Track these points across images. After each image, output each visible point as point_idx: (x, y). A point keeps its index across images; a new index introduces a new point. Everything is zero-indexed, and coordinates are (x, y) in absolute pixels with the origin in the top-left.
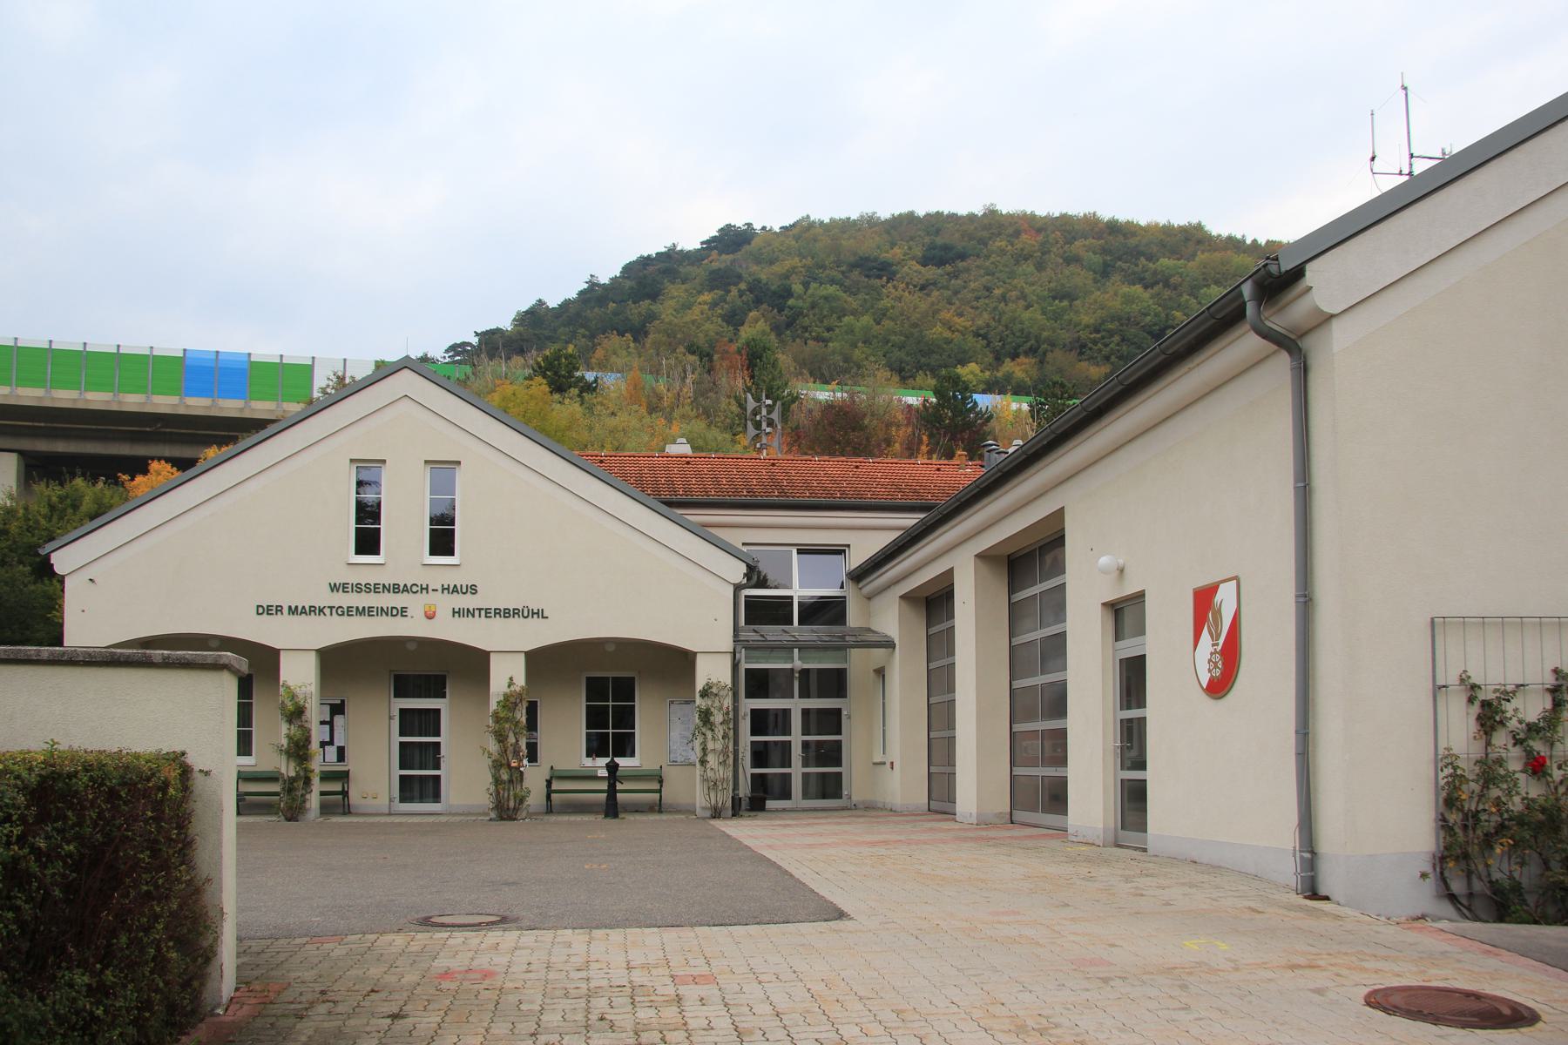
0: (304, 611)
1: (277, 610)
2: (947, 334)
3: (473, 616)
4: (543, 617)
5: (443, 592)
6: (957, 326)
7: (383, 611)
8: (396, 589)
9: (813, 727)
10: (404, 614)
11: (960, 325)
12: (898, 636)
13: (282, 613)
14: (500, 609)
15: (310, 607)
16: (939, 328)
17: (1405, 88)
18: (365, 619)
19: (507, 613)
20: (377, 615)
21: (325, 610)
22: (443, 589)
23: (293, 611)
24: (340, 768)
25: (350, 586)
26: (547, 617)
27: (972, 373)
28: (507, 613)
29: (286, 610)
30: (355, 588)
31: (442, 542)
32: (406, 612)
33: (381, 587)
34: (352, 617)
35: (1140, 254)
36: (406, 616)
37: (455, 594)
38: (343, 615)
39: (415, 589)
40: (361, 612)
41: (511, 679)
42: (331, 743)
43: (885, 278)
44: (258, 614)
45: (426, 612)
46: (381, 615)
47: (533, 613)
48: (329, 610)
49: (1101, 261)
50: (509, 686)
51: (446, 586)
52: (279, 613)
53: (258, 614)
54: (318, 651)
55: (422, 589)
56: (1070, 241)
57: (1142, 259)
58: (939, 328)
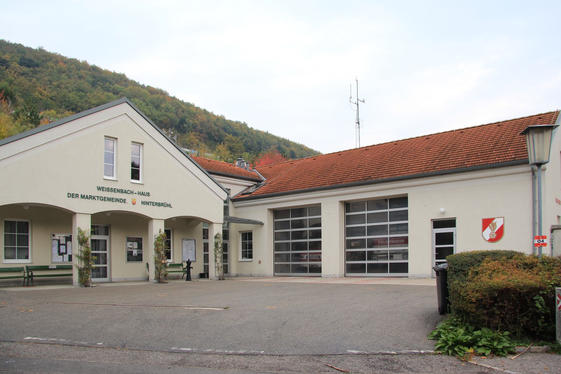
0: (87, 198)
1: (76, 196)
2: (40, 96)
3: (149, 205)
4: (171, 207)
5: (138, 194)
6: (44, 94)
7: (117, 200)
8: (121, 191)
9: (94, 249)
10: (125, 202)
11: (45, 94)
12: (499, 228)
13: (78, 198)
14: (157, 203)
15: (90, 196)
16: (37, 93)
17: (357, 81)
18: (118, 203)
19: (159, 205)
20: (115, 201)
21: (95, 198)
22: (138, 193)
23: (83, 197)
24: (69, 264)
25: (105, 188)
26: (172, 207)
27: (53, 114)
28: (159, 205)
29: (80, 196)
30: (107, 190)
31: (135, 174)
32: (125, 201)
33: (116, 190)
34: (74, 198)
35: (107, 81)
36: (126, 203)
37: (142, 195)
38: (103, 200)
39: (129, 192)
40: (110, 199)
41: (160, 230)
42: (66, 253)
43: (5, 67)
44: (68, 197)
45: (133, 202)
46: (117, 202)
47: (168, 205)
48: (97, 197)
49: (92, 80)
50: (160, 232)
51: (139, 192)
52: (77, 197)
53: (68, 197)
54: (92, 215)
55: (131, 192)
56: (79, 69)
57: (108, 83)
58: (37, 93)
